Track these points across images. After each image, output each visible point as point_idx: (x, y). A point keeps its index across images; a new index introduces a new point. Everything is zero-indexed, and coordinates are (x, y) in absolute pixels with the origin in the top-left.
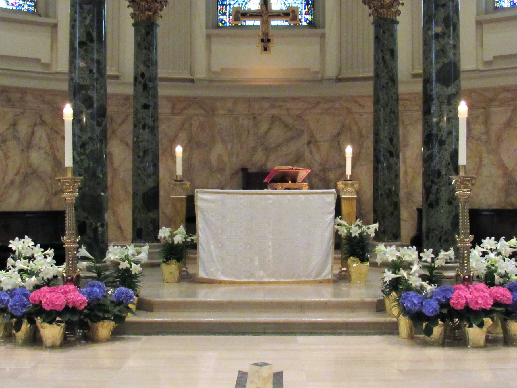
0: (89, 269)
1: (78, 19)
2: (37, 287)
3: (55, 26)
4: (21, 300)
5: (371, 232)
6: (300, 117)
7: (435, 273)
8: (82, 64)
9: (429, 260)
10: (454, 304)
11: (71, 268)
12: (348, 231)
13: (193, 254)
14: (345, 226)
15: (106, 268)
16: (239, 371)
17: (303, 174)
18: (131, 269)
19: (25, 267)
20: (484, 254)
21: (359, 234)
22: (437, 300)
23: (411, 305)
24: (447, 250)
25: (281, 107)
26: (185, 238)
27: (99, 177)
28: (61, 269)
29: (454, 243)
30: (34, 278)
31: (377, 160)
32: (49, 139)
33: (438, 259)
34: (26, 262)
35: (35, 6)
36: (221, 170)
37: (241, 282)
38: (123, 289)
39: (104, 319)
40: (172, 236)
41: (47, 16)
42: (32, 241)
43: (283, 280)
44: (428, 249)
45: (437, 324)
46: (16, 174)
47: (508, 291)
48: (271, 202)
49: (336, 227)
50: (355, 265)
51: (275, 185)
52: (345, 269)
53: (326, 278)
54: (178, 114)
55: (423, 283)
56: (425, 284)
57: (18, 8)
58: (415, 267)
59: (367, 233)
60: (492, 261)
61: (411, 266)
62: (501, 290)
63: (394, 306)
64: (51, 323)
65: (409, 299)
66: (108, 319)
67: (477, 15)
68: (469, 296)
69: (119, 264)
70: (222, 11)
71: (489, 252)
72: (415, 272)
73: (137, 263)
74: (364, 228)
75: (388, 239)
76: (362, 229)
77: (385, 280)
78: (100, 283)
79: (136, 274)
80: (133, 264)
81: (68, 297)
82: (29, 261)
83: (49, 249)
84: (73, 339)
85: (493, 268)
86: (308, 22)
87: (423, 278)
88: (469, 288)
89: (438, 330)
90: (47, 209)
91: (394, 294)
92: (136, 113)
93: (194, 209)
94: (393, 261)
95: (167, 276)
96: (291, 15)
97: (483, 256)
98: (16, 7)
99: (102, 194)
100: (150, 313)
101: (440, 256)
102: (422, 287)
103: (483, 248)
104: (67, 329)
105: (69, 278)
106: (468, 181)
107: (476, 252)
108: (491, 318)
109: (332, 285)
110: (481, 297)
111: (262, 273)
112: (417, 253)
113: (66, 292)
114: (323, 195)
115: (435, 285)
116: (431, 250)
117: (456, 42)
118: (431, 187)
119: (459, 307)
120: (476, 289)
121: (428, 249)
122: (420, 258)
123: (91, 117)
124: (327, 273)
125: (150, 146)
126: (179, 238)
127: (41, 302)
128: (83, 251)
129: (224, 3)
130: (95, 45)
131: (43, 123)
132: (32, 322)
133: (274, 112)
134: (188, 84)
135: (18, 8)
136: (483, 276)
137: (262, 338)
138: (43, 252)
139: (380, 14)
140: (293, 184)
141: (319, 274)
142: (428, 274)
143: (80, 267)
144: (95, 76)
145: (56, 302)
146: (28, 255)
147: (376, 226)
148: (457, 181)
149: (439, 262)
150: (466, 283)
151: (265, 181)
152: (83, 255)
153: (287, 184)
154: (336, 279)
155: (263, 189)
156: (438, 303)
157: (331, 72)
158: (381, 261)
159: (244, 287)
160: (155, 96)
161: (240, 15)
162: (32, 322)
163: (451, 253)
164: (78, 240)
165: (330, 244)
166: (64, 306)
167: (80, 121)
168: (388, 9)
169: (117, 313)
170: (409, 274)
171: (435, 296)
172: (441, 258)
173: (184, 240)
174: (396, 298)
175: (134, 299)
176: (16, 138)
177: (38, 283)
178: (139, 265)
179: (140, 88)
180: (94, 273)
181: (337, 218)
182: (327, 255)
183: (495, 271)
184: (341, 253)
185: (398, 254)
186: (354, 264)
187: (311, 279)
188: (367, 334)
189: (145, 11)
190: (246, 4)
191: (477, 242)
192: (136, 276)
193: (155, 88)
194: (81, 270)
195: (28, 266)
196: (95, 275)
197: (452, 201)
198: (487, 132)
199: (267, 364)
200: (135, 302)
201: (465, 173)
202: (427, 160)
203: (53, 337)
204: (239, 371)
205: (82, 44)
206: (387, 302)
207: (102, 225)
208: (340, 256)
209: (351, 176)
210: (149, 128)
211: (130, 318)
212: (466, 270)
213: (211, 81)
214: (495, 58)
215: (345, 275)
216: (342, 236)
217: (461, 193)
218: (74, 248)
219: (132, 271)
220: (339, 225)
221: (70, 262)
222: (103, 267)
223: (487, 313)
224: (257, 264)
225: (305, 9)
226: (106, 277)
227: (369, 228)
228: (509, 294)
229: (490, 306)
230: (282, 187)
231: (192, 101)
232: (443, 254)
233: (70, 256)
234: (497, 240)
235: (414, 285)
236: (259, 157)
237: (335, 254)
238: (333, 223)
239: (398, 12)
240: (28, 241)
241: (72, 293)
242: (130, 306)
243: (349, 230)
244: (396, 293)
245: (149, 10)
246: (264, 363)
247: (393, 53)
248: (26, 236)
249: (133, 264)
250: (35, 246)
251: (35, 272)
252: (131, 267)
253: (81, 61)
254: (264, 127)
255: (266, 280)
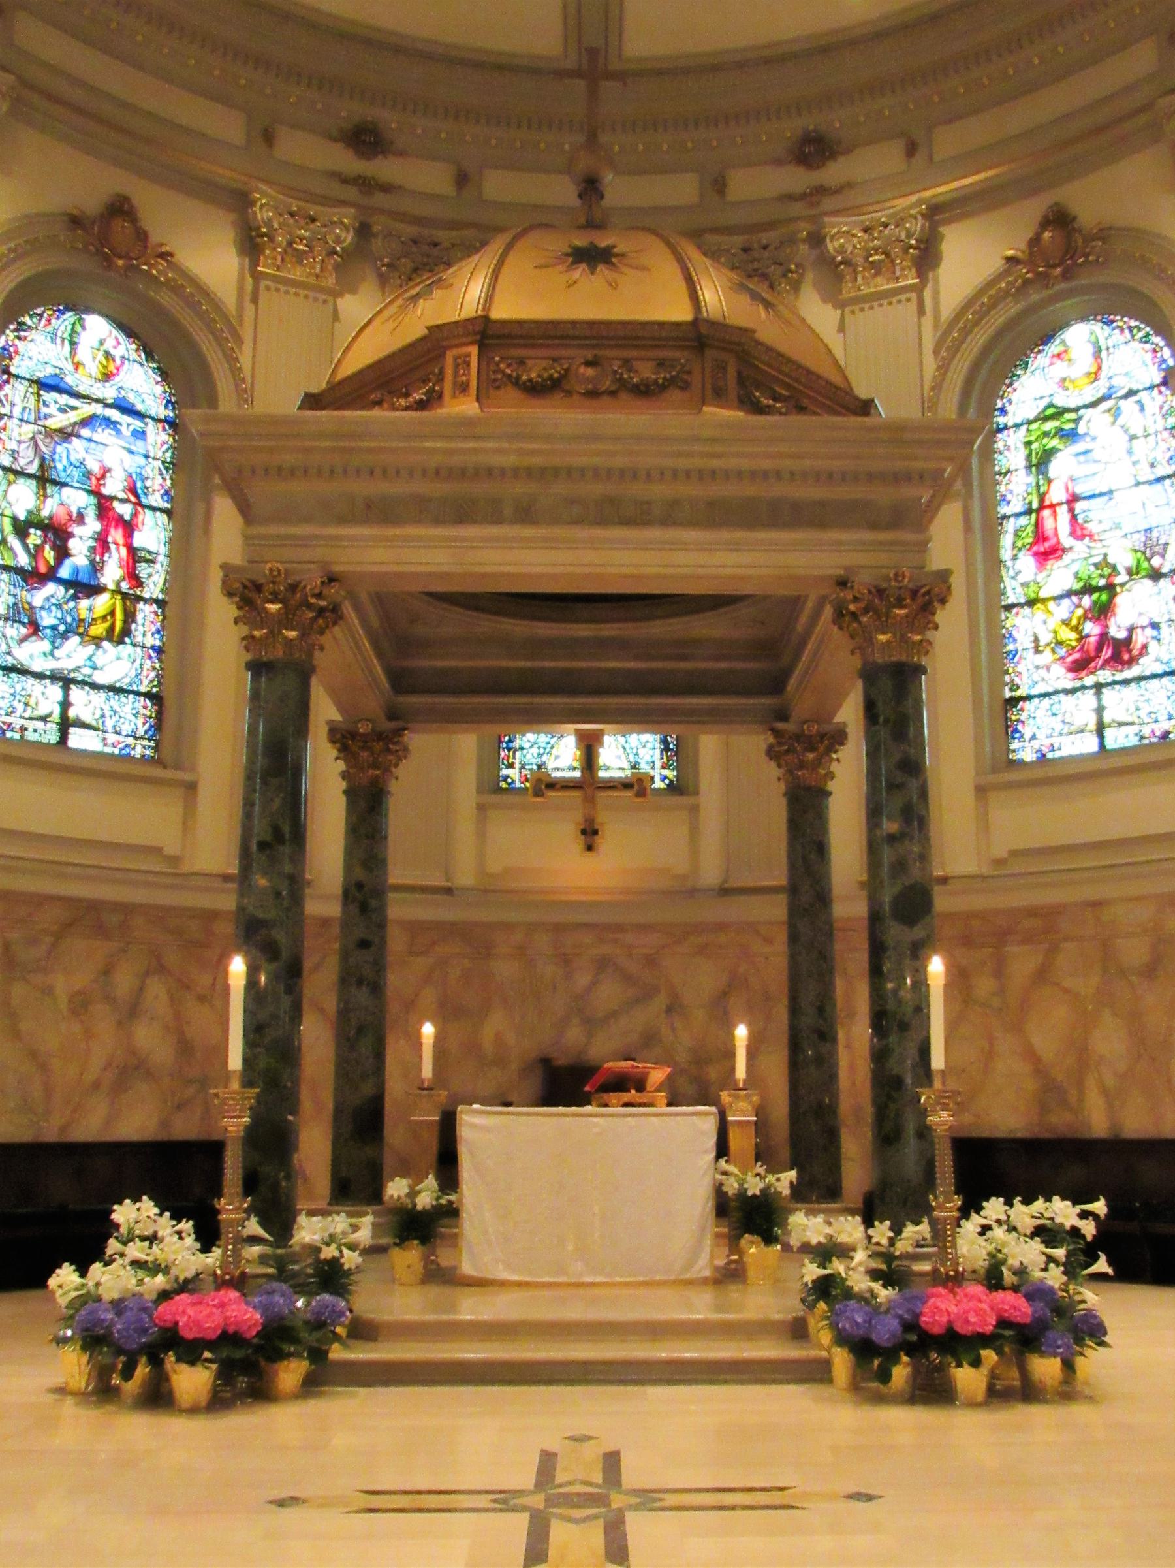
0: (263, 1259)
1: (257, 801)
2: (164, 1295)
3: (191, 788)
4: (140, 1320)
5: (784, 1188)
6: (651, 961)
7: (897, 1266)
8: (263, 882)
9: (884, 1242)
10: (927, 1323)
11: (230, 1259)
12: (741, 1185)
13: (447, 1227)
14: (736, 1175)
15: (294, 1258)
16: (542, 1451)
17: (657, 1076)
18: (342, 1261)
19: (143, 1257)
20: (985, 1229)
21: (761, 1190)
22: (900, 1317)
23: (852, 1327)
24: (917, 1223)
25: (616, 941)
26: (438, 1199)
27: (285, 1087)
28: (213, 1259)
29: (928, 1210)
30: (160, 1279)
31: (795, 1046)
32: (172, 1000)
33: (900, 1240)
34: (144, 1246)
35: (156, 749)
36: (500, 1061)
37: (540, 1283)
38: (327, 1297)
39: (290, 1355)
40: (413, 1194)
41: (178, 767)
42: (155, 1206)
43: (618, 1279)
44: (881, 1222)
45: (897, 1361)
46: (105, 1069)
47: (1023, 1299)
48: (596, 1130)
49: (719, 1177)
50: (753, 1250)
51: (605, 1096)
52: (736, 1257)
53: (699, 1276)
54: (422, 953)
55: (873, 1284)
56: (877, 1286)
57: (123, 752)
58: (860, 1256)
59: (775, 1189)
60: (997, 1244)
61: (852, 1254)
62: (1010, 1296)
63: (822, 1328)
64: (192, 1363)
65: (848, 1314)
66: (297, 1355)
67: (977, 775)
68: (953, 1309)
69: (319, 1250)
70: (508, 761)
71: (994, 1225)
72: (860, 1264)
73: (352, 1247)
74: (771, 1178)
75: (817, 1198)
76: (767, 1180)
77: (805, 1280)
78: (284, 1286)
79: (350, 1269)
80: (346, 1251)
81: (228, 1314)
82: (151, 1243)
83: (185, 1220)
84: (229, 1395)
85: (1000, 1256)
86: (667, 781)
87: (875, 1275)
88: (955, 1294)
89: (901, 1373)
90: (162, 1136)
91: (822, 1305)
92: (345, 956)
93: (455, 1141)
94: (820, 1243)
95: (401, 1273)
96: (636, 787)
97: (981, 1234)
98: (121, 750)
99: (290, 1118)
100: (371, 1345)
101: (904, 1235)
102: (871, 1291)
103: (986, 1218)
104: (220, 1375)
105: (227, 1277)
106: (948, 1097)
107: (971, 1226)
108: (995, 1350)
109: (710, 1288)
110: (975, 1311)
111: (580, 1266)
112: (862, 1228)
113: (222, 1305)
114: (694, 1118)
115: (894, 1289)
116: (888, 1223)
117: (924, 848)
118: (886, 1106)
119: (936, 1330)
120: (966, 1295)
121: (881, 1222)
122: (869, 1238)
123: (274, 977)
124: (703, 1267)
125: (370, 1018)
126: (425, 1199)
127: (177, 1323)
128: (253, 1227)
129: (511, 745)
130: (286, 849)
131: (161, 969)
132: (156, 1362)
133: (606, 949)
134: (439, 897)
135: (123, 752)
136: (982, 1272)
137: (578, 1390)
138: (173, 1226)
139: (798, 778)
140: (639, 1094)
141: (688, 1266)
142: (884, 1267)
143: (247, 1256)
144: (286, 903)
145: (207, 1323)
146: (146, 1233)
147: (792, 1174)
148: (929, 1098)
149: (902, 1247)
150: (950, 1284)
151: (587, 1088)
152: (251, 1233)
153: (628, 1094)
154: (718, 1275)
155: (583, 1105)
156: (899, 1323)
157: (711, 874)
158: (799, 1244)
159: (545, 1293)
160: (382, 925)
161: (543, 787)
162: (156, 1362)
163: (924, 1228)
164: (246, 1205)
165: (708, 1210)
166: (219, 1332)
167: (257, 982)
168: (813, 769)
169: (315, 1344)
170: (848, 1268)
171: (894, 1309)
172: (907, 1239)
173: (434, 1203)
174: (826, 1312)
175: (347, 1317)
176: (109, 999)
177: (168, 1287)
178: (358, 1252)
179: (354, 909)
180: (272, 1267)
181: (720, 1160)
182: (703, 1230)
183: (1004, 1262)
184: (729, 1226)
185: (828, 1230)
186: (753, 1248)
187: (672, 1278)
188: (774, 1382)
189: (368, 767)
190: (552, 747)
191: (971, 1206)
192: (348, 1273)
193: (382, 908)
194: (248, 1261)
195: (147, 1255)
196: (271, 1270)
197: (924, 1133)
198: (1001, 991)
199: (591, 1438)
200: (347, 1322)
201: (944, 1084)
202: (880, 1056)
203: (196, 1389)
204: (542, 1451)
205: (263, 846)
206: (812, 1322)
207: (288, 1177)
208: (726, 1230)
209: (745, 1081)
210: (368, 984)
211: (337, 1353)
212: (950, 1259)
213: (486, 891)
214: (1014, 854)
215: (736, 1269)
216: (730, 1193)
217: (941, 1119)
218: (238, 1220)
219: (343, 1265)
220: (725, 1173)
221: (230, 1247)
222: (287, 1255)
223: (985, 1340)
224: (571, 1247)
225: (662, 758)
226: (295, 1275)
227: (778, 1180)
228: (1026, 1304)
229: (991, 1328)
230: (619, 1101)
231: (451, 930)
232: (910, 1230)
233: (231, 1235)
234: (1009, 1203)
235: (856, 1289)
236: (574, 1035)
237: (717, 1226)
238: (713, 1169)
239: (830, 776)
240: (148, 1206)
241: (234, 1307)
242: (339, 1329)
243: (742, 1182)
244: (826, 1303)
245: (375, 766)
246: (585, 1436)
247: (822, 848)
248: (145, 1198)
249: (346, 1251)
250: (161, 1215)
251: (163, 1266)
252: (342, 1256)
253: (263, 877)
254: (583, 980)
255: (588, 1279)
